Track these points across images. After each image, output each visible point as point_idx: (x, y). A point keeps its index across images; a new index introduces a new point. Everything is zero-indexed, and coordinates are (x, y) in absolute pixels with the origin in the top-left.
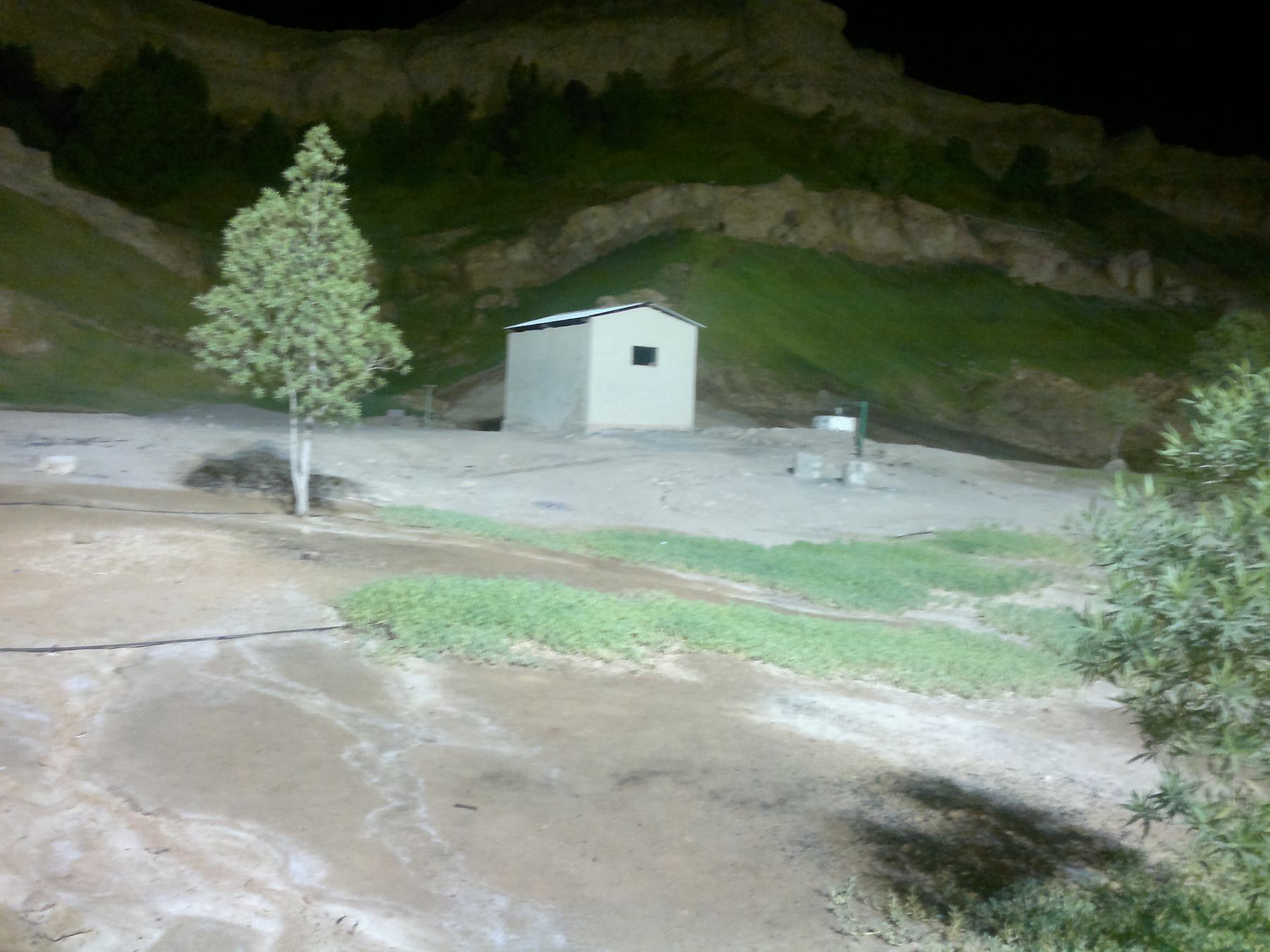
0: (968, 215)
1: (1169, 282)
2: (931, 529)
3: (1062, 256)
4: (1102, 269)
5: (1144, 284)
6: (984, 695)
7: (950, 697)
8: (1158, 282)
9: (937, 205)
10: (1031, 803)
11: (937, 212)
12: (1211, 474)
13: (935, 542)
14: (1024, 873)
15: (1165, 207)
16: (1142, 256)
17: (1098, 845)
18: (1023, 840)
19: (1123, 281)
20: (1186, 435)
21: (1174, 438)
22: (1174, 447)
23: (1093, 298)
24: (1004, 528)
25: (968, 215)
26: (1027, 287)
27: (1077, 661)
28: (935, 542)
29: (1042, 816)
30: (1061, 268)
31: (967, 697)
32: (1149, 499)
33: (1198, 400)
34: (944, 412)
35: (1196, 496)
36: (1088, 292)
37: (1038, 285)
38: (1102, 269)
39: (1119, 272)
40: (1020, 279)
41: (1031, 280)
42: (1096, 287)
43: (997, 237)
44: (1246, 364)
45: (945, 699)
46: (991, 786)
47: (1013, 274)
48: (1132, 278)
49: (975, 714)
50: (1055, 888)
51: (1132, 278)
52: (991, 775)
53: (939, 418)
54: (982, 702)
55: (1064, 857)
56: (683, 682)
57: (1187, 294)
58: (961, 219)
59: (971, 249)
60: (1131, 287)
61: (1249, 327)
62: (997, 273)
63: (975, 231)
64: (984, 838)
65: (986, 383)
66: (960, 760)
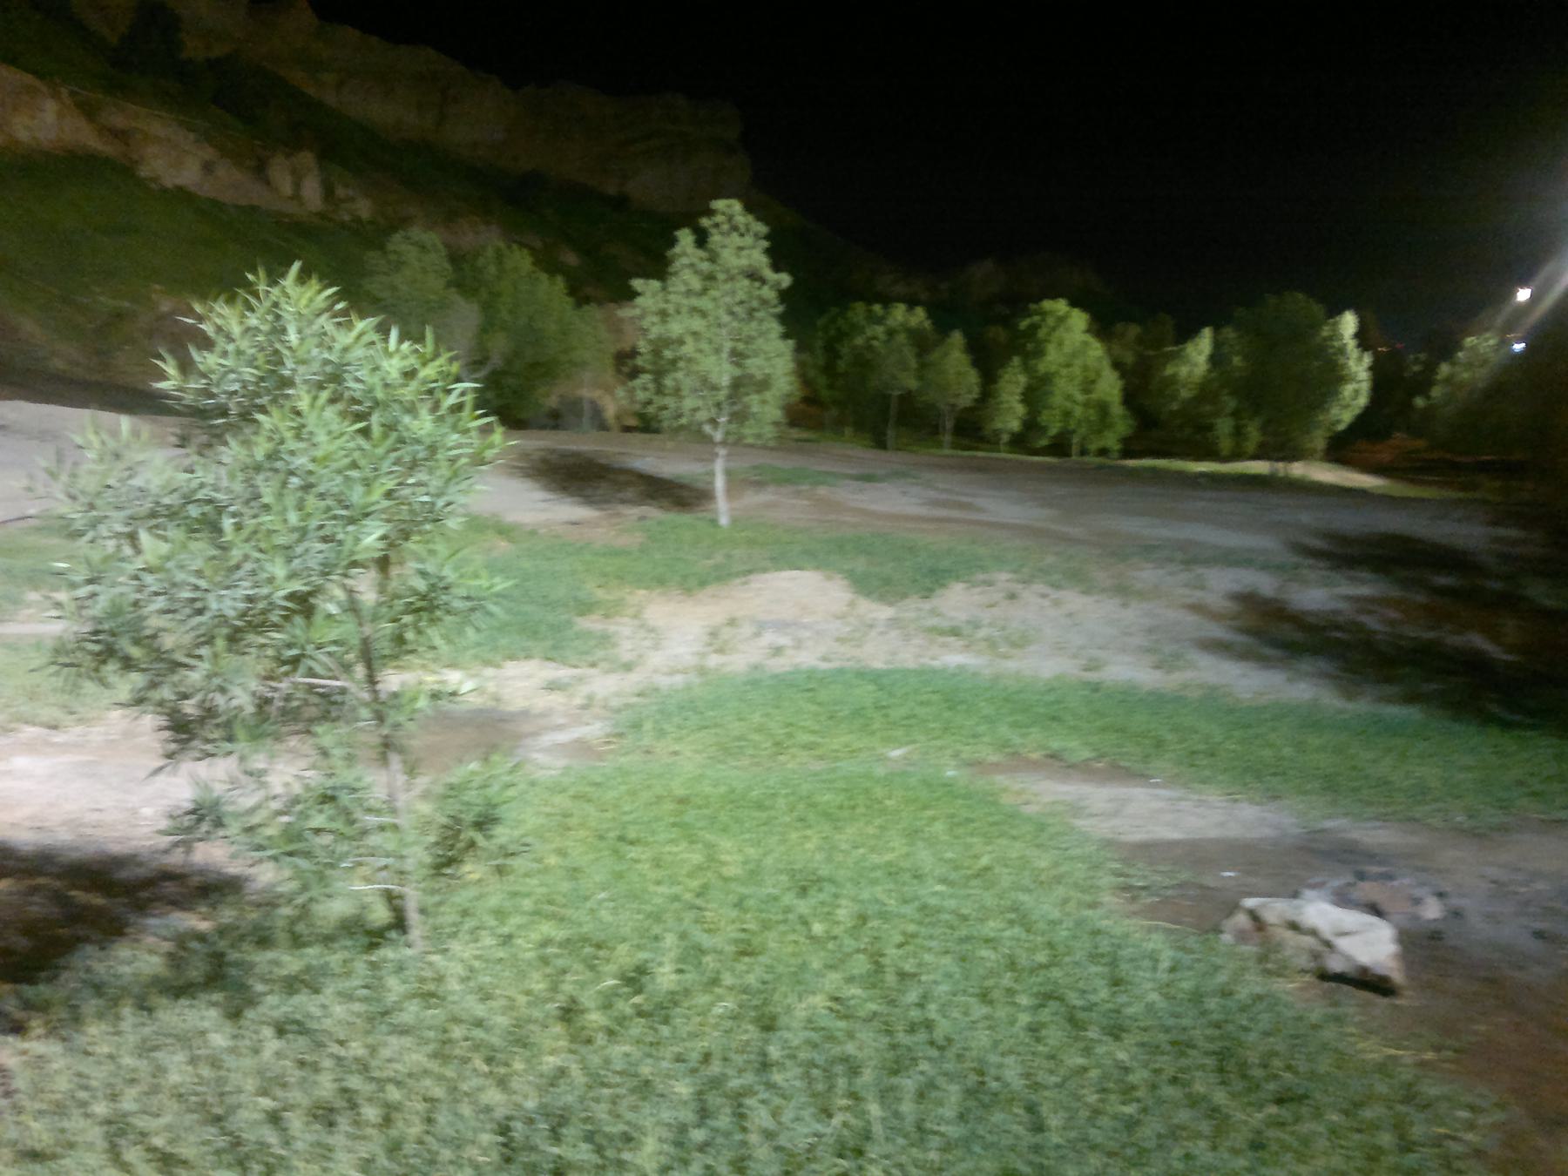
0: (76, 89)
1: (340, 192)
2: (32, 512)
3: (208, 153)
4: (260, 169)
5: (312, 191)
6: (80, 721)
7: (30, 731)
8: (329, 193)
9: (26, 70)
10: (116, 849)
11: (29, 79)
12: (223, 412)
13: (38, 530)
14: (79, 940)
15: (331, 99)
16: (307, 158)
17: (196, 880)
18: (98, 900)
19: (287, 188)
20: (186, 366)
21: (170, 368)
22: (170, 381)
23: (254, 209)
24: (166, 501)
25: (76, 89)
26: (164, 190)
27: (53, 663)
28: (38, 530)
29: (120, 862)
30: (208, 168)
31: (55, 728)
32: (127, 446)
33: (200, 319)
34: (64, 355)
35: (218, 437)
36: (243, 202)
37: (180, 189)
38: (260, 169)
39: (280, 173)
40: (155, 180)
41: (169, 182)
42: (256, 194)
43: (118, 121)
44: (262, 273)
45: (21, 735)
46: (62, 837)
47: (144, 172)
48: (297, 185)
49: (64, 748)
50: (123, 951)
51: (297, 185)
52: (64, 823)
53: (58, 364)
54: (79, 729)
55: (142, 908)
56: (1505, 662)
57: (364, 208)
58: (64, 91)
59: (86, 137)
60: (296, 197)
61: (423, 248)
62: (125, 171)
63: (89, 111)
64: (38, 908)
65: (119, 316)
66: (19, 814)
